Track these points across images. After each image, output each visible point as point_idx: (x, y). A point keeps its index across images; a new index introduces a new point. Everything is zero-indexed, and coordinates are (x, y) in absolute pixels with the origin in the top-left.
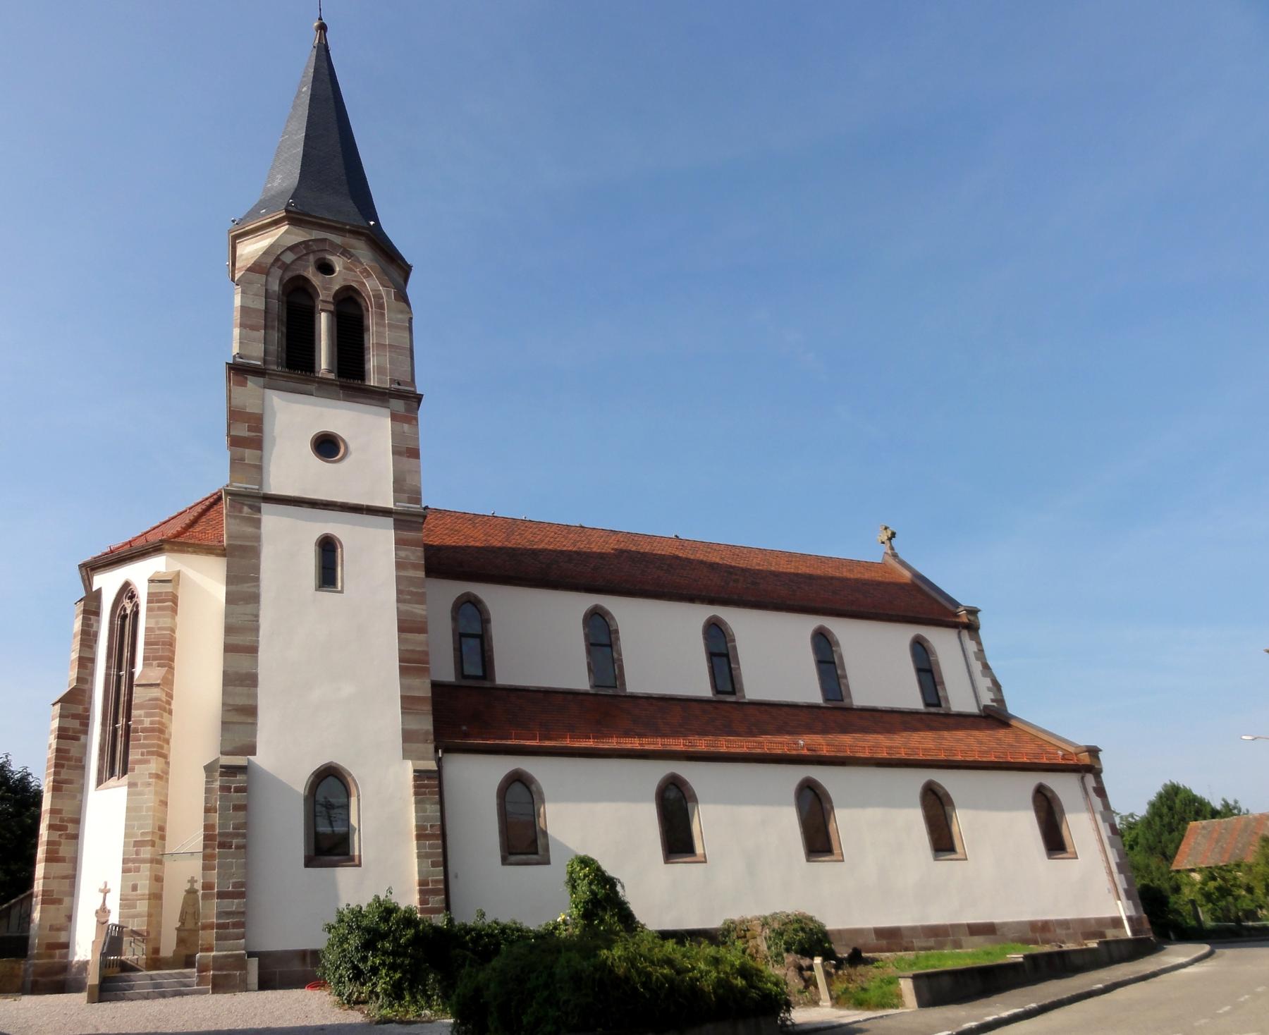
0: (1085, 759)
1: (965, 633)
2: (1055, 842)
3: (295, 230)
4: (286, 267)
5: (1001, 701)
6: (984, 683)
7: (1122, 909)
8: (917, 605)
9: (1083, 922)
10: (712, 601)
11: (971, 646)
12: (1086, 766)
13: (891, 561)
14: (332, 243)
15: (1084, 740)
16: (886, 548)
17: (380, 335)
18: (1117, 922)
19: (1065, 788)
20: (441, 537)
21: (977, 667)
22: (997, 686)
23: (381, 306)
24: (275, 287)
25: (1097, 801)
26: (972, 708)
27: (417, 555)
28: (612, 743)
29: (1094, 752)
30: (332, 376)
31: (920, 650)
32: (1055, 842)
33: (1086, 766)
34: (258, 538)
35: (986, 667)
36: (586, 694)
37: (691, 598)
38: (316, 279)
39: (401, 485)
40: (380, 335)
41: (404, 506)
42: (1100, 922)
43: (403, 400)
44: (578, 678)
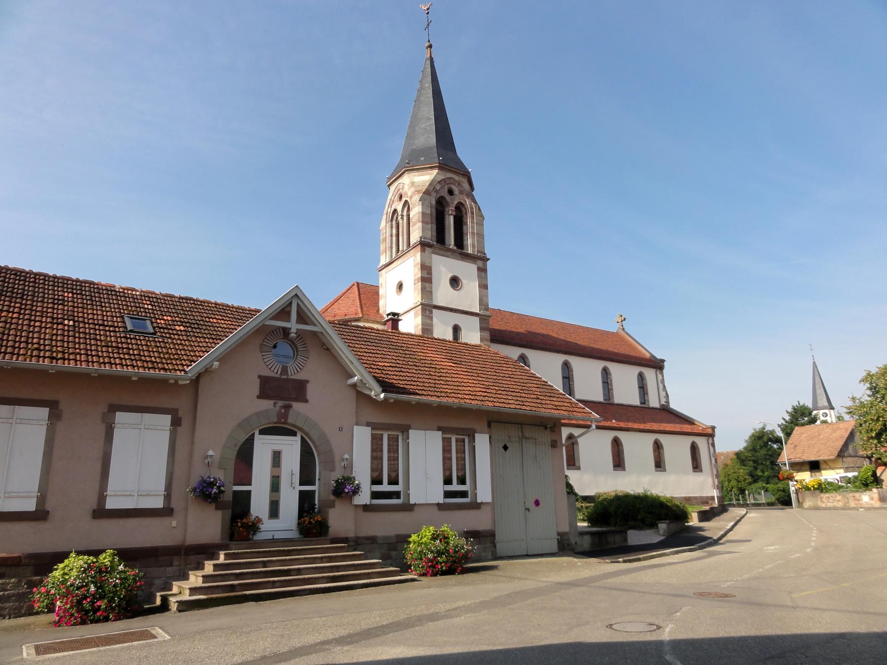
0: (710, 431)
1: (658, 372)
2: (697, 466)
3: (441, 172)
4: (437, 192)
5: (668, 402)
6: (663, 394)
7: (715, 493)
8: (613, 352)
9: (702, 497)
10: (566, 353)
11: (660, 377)
12: (709, 434)
13: (622, 332)
14: (454, 180)
15: (709, 424)
16: (619, 325)
17: (473, 228)
18: (713, 498)
19: (701, 442)
20: (495, 325)
21: (661, 386)
22: (667, 396)
23: (472, 213)
24: (434, 203)
25: (711, 448)
26: (657, 405)
27: (487, 335)
28: (648, 426)
29: (713, 428)
30: (455, 248)
31: (641, 376)
32: (697, 466)
33: (709, 434)
34: (432, 325)
35: (664, 387)
36: (637, 407)
37: (558, 352)
38: (448, 198)
39: (483, 303)
40: (473, 228)
41: (482, 313)
42: (707, 497)
43: (480, 259)
44: (636, 401)
